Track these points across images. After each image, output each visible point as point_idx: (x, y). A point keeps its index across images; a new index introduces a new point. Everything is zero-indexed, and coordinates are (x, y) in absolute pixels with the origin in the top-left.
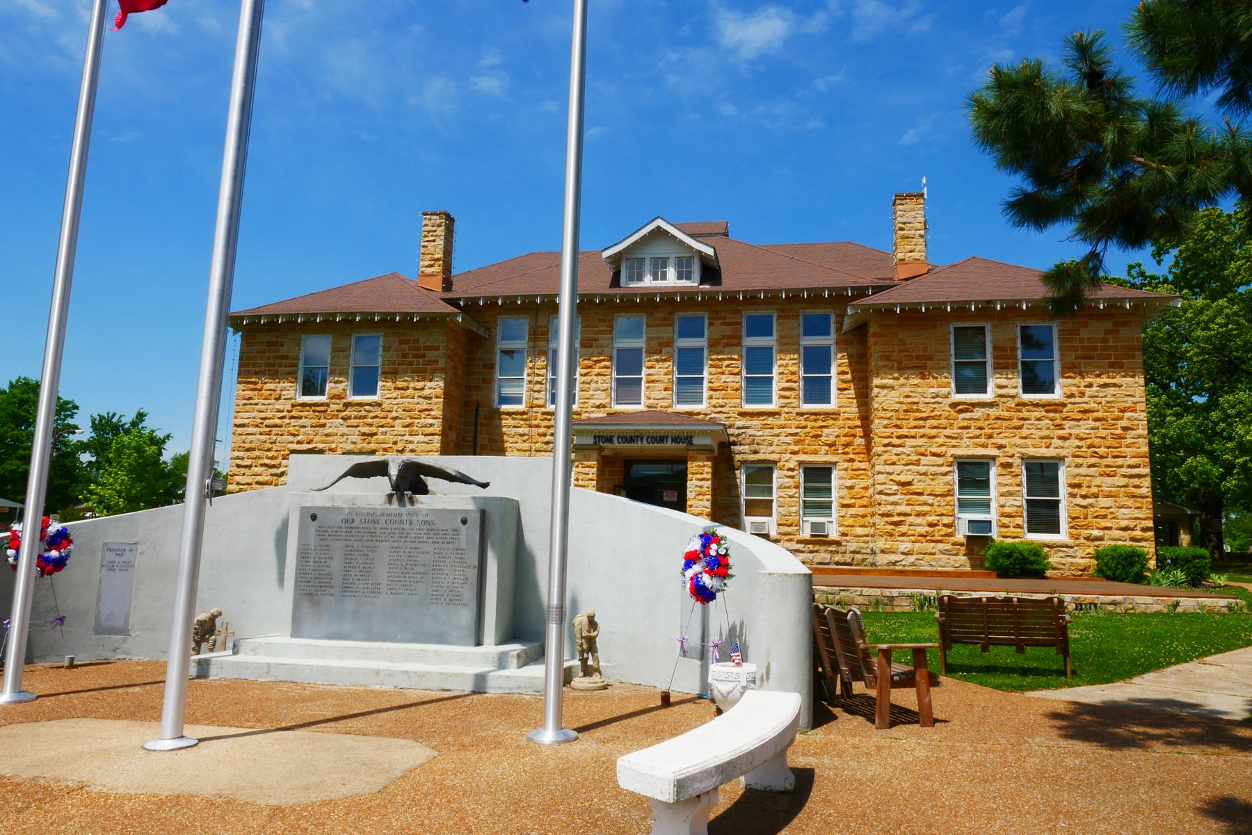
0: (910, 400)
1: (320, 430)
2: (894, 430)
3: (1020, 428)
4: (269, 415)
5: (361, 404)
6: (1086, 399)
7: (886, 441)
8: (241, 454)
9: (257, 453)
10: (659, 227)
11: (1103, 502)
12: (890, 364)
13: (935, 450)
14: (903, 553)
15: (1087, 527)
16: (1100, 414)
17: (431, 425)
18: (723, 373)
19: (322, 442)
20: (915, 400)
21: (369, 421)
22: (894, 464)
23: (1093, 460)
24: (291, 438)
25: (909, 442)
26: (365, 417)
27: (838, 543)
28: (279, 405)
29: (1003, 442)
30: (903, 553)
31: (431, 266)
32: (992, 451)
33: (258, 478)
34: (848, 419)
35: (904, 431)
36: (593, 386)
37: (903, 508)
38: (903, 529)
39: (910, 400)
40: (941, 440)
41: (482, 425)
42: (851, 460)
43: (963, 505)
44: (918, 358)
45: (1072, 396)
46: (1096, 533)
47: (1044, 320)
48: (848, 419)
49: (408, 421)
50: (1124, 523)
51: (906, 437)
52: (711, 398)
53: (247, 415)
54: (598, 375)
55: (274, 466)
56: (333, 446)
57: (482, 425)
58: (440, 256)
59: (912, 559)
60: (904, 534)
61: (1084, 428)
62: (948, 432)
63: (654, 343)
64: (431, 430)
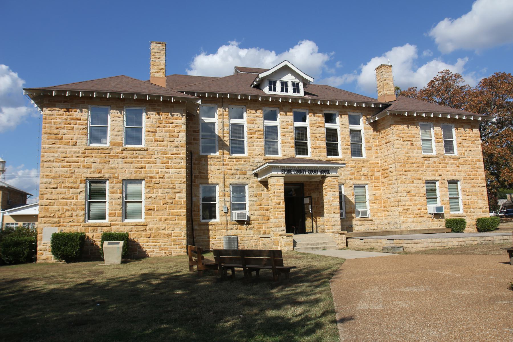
0: (408, 155)
1: (106, 165)
2: (403, 168)
3: (446, 167)
4: (68, 154)
5: (133, 150)
6: (465, 156)
7: (401, 173)
8: (49, 180)
9: (61, 179)
10: (286, 65)
11: (474, 198)
12: (399, 138)
13: (418, 176)
14: (410, 223)
15: (470, 208)
16: (470, 162)
17: (179, 163)
18: (318, 140)
19: (108, 173)
20: (410, 155)
21: (139, 159)
22: (404, 183)
23: (469, 181)
24: (86, 170)
25: (409, 173)
26: (137, 157)
27: (371, 220)
28: (75, 149)
29: (442, 173)
30: (410, 223)
31: (158, 72)
32: (437, 178)
33: (63, 196)
34: (372, 163)
35: (406, 168)
36: (255, 144)
37: (409, 203)
38: (409, 212)
39: (408, 155)
40: (420, 172)
41: (195, 164)
42: (374, 182)
43: (34, 218)
44: (409, 137)
45: (461, 154)
46: (472, 210)
47: (450, 123)
48: (372, 163)
49: (165, 160)
50: (480, 206)
51: (408, 171)
52: (313, 152)
53: (52, 154)
54: (257, 138)
55: (75, 188)
56: (116, 175)
57: (195, 164)
58: (163, 67)
59: (414, 225)
60: (410, 214)
61: (466, 167)
62: (422, 169)
63: (285, 124)
64: (179, 166)
